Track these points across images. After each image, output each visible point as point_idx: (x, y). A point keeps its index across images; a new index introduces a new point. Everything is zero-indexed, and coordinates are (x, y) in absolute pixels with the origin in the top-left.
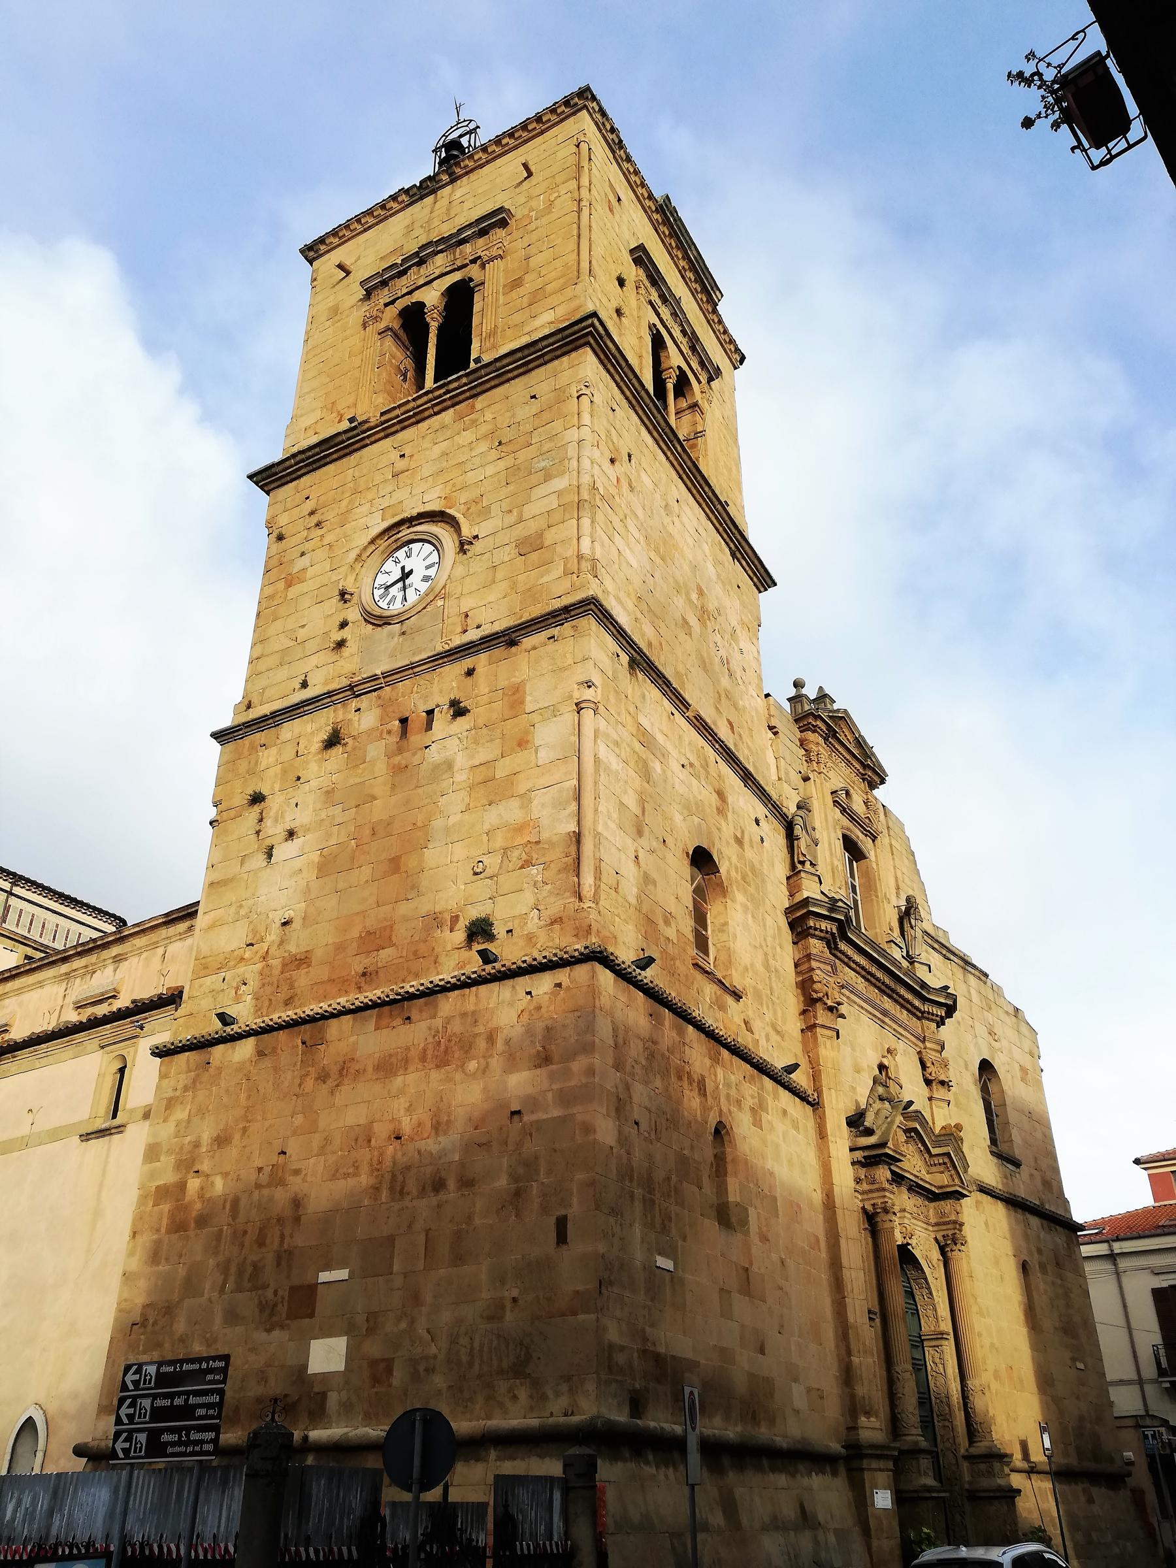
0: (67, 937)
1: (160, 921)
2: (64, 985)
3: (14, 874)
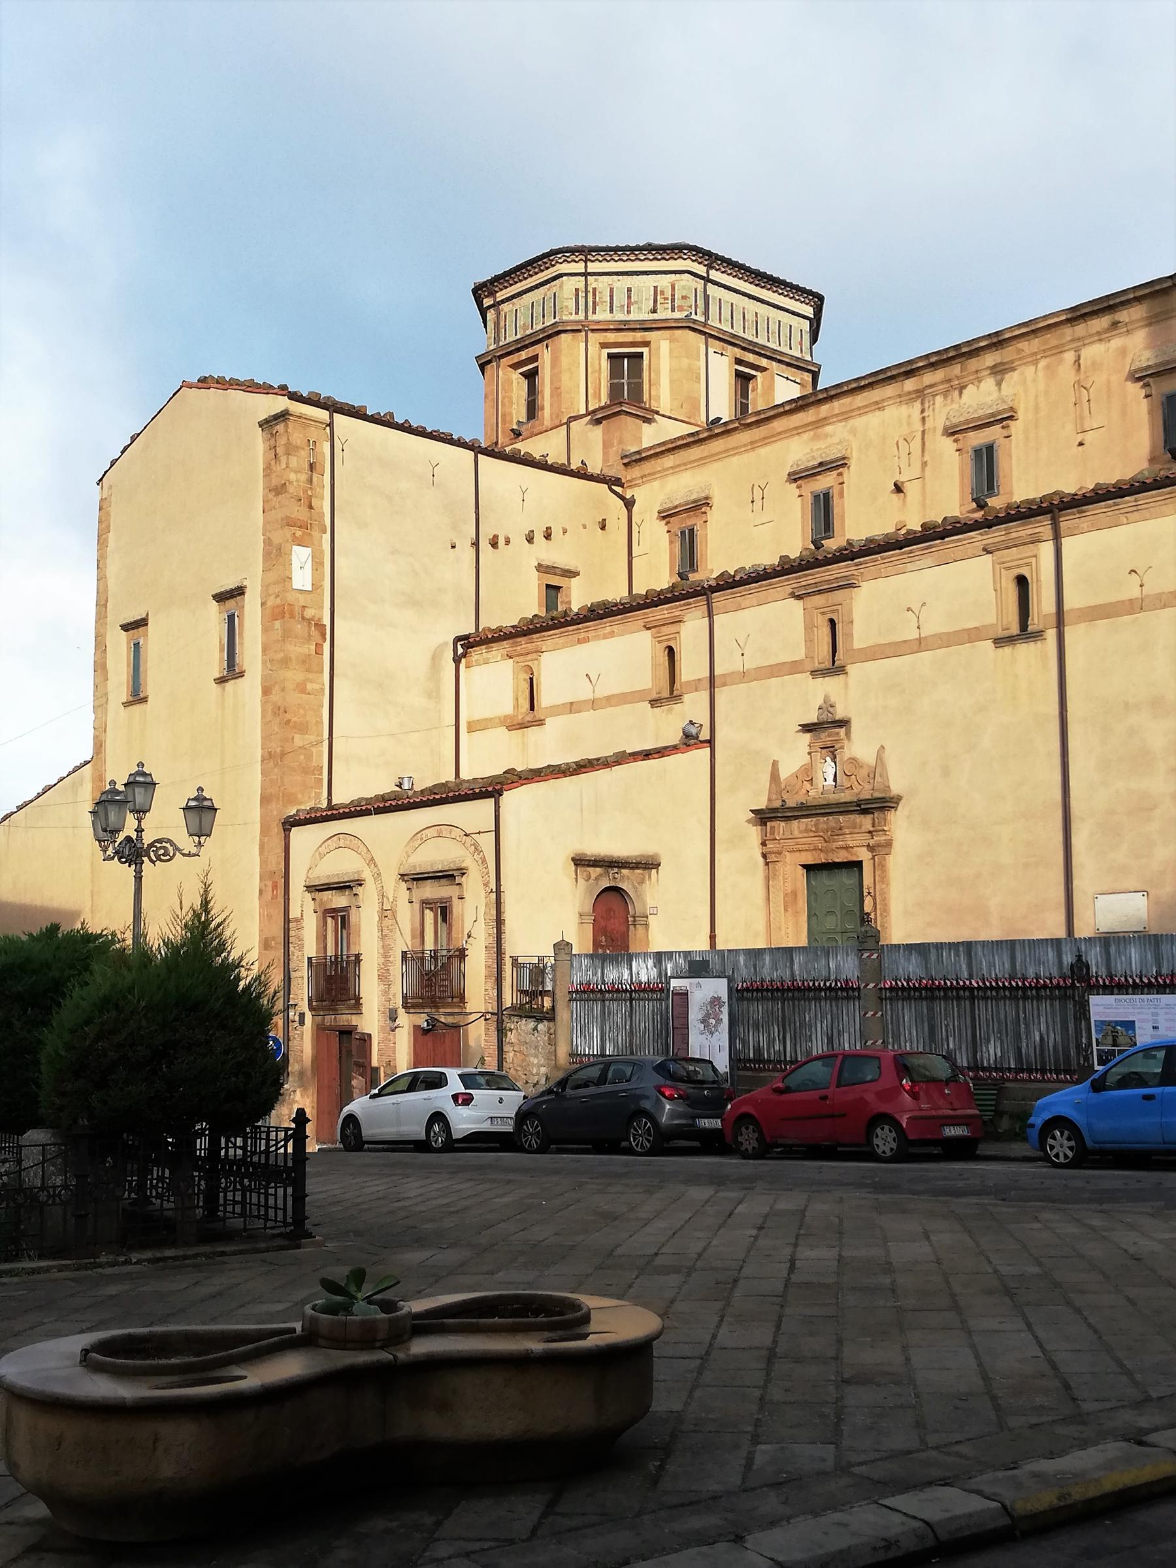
1: (1063, 318)
2: (917, 405)
3: (708, 254)
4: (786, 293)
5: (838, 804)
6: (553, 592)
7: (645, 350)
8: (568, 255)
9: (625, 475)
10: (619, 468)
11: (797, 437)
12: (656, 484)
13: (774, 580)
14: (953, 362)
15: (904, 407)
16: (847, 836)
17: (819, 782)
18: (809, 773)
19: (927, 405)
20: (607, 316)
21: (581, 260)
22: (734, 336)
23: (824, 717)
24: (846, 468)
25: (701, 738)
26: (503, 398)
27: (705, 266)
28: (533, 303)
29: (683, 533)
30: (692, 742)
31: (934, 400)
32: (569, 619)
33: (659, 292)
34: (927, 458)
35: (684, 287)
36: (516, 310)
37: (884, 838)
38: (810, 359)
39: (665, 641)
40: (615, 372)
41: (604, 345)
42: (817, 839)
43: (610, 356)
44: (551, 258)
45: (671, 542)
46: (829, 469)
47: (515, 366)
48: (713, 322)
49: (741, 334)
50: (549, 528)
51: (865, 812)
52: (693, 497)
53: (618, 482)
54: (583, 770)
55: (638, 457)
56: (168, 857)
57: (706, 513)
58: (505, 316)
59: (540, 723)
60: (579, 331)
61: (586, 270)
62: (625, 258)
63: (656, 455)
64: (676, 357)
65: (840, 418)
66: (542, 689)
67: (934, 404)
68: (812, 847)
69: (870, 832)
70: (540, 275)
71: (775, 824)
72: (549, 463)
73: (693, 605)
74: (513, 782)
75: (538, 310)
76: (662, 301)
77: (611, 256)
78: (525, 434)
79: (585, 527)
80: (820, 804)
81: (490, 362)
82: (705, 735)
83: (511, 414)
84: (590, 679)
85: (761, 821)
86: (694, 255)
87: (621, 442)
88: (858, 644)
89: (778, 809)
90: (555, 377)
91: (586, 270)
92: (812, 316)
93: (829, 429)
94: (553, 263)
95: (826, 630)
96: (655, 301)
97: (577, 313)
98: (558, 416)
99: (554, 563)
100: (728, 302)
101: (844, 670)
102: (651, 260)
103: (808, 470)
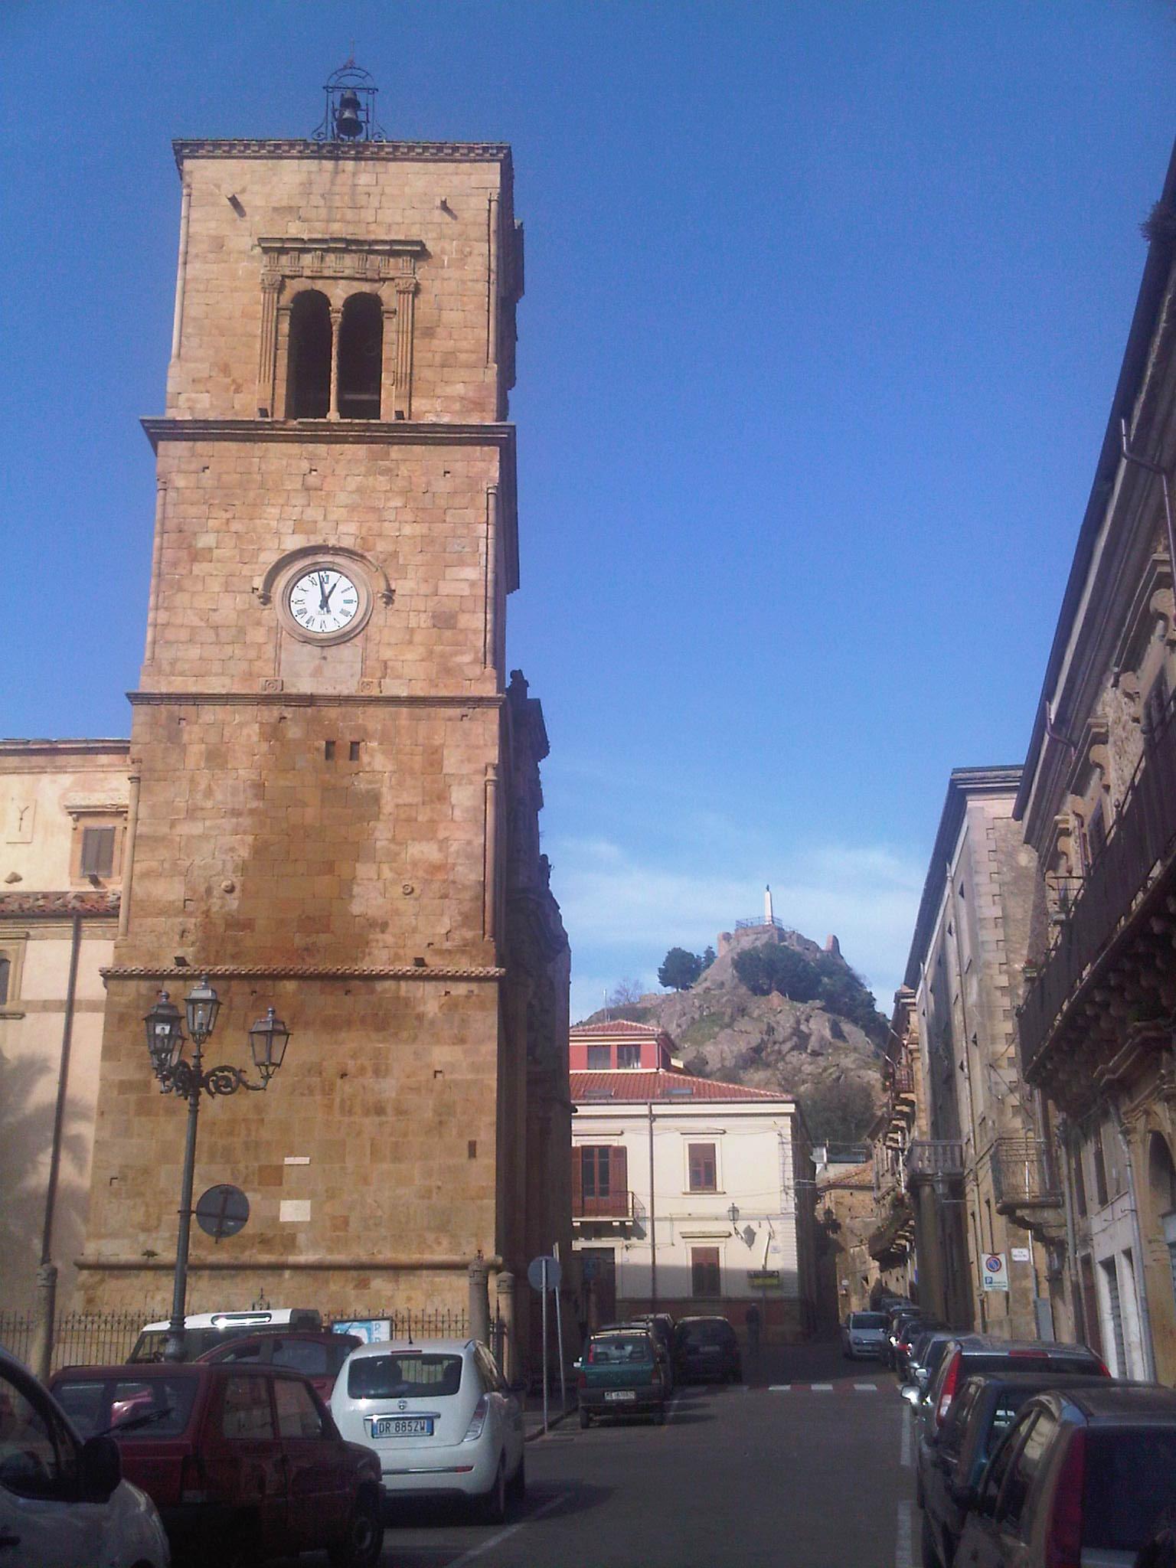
56: (229, 1089)
103: (13, 744)
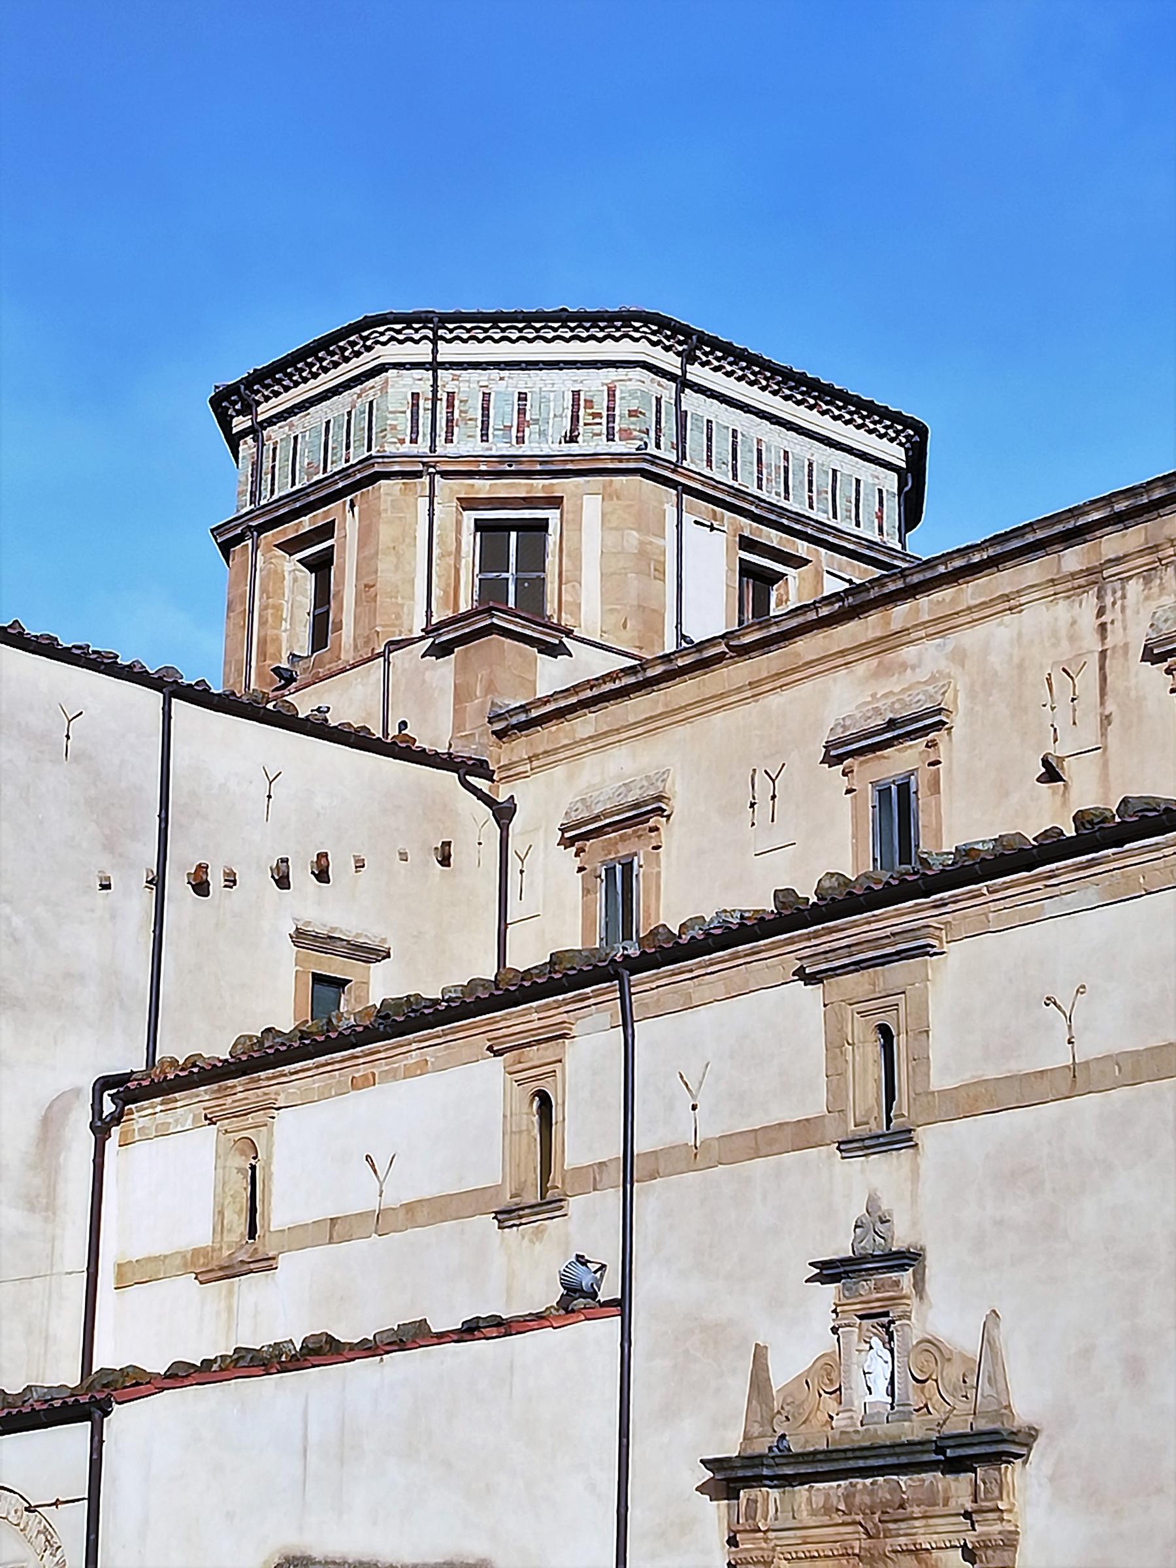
0: (810, 483)
2: (1090, 600)
3: (687, 331)
4: (848, 417)
5: (895, 1447)
6: (328, 992)
7: (552, 515)
8: (398, 327)
9: (497, 755)
10: (484, 740)
11: (843, 672)
12: (559, 771)
13: (762, 942)
14: (1162, 512)
15: (1062, 604)
16: (917, 1523)
17: (858, 1398)
18: (834, 1376)
19: (1109, 599)
20: (475, 447)
21: (425, 337)
22: (738, 493)
23: (869, 1246)
24: (944, 732)
25: (602, 1298)
26: (264, 608)
27: (678, 354)
28: (328, 423)
29: (610, 871)
30: (580, 1302)
31: (1123, 588)
32: (333, 1035)
33: (582, 403)
34: (1110, 707)
35: (632, 394)
36: (296, 438)
37: (998, 1527)
38: (899, 547)
39: (536, 1078)
40: (491, 558)
41: (468, 504)
42: (850, 1529)
43: (480, 525)
44: (365, 334)
45: (586, 891)
46: (908, 734)
47: (290, 547)
48: (695, 462)
49: (753, 490)
50: (323, 856)
51: (955, 1466)
52: (631, 798)
53: (481, 768)
54: (313, 1359)
55: (523, 717)
57: (657, 829)
58: (275, 449)
59: (267, 1264)
60: (417, 475)
61: (434, 358)
62: (514, 335)
63: (560, 714)
64: (616, 529)
65: (931, 630)
66: (274, 1191)
67: (1124, 597)
68: (838, 1549)
69: (967, 1515)
70: (344, 367)
71: (755, 1493)
72: (332, 723)
73: (592, 1001)
74: (137, 1384)
75: (338, 436)
76: (590, 420)
77: (486, 330)
78: (301, 678)
79: (404, 857)
80: (856, 1445)
81: (239, 539)
82: (610, 1289)
83: (277, 640)
84: (373, 1166)
85: (728, 1488)
86: (654, 333)
87: (490, 688)
88: (939, 1081)
89: (761, 1456)
90: (366, 565)
91: (434, 358)
92: (904, 465)
93: (908, 653)
94: (369, 343)
95: (873, 1049)
96: (575, 419)
97: (414, 441)
98: (367, 642)
99: (334, 929)
100: (728, 428)
101: (911, 1139)
102: (567, 340)
